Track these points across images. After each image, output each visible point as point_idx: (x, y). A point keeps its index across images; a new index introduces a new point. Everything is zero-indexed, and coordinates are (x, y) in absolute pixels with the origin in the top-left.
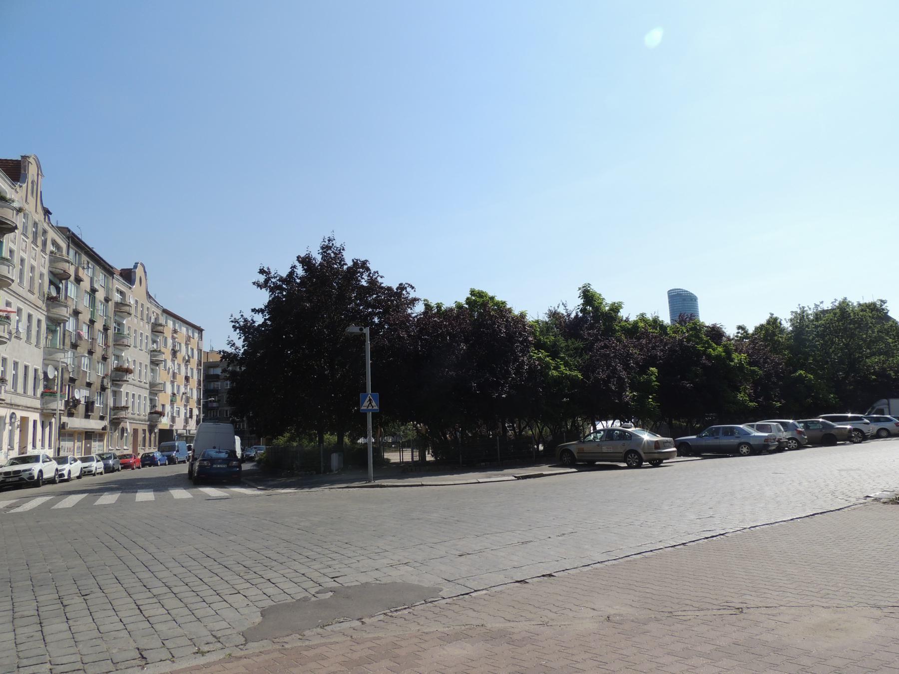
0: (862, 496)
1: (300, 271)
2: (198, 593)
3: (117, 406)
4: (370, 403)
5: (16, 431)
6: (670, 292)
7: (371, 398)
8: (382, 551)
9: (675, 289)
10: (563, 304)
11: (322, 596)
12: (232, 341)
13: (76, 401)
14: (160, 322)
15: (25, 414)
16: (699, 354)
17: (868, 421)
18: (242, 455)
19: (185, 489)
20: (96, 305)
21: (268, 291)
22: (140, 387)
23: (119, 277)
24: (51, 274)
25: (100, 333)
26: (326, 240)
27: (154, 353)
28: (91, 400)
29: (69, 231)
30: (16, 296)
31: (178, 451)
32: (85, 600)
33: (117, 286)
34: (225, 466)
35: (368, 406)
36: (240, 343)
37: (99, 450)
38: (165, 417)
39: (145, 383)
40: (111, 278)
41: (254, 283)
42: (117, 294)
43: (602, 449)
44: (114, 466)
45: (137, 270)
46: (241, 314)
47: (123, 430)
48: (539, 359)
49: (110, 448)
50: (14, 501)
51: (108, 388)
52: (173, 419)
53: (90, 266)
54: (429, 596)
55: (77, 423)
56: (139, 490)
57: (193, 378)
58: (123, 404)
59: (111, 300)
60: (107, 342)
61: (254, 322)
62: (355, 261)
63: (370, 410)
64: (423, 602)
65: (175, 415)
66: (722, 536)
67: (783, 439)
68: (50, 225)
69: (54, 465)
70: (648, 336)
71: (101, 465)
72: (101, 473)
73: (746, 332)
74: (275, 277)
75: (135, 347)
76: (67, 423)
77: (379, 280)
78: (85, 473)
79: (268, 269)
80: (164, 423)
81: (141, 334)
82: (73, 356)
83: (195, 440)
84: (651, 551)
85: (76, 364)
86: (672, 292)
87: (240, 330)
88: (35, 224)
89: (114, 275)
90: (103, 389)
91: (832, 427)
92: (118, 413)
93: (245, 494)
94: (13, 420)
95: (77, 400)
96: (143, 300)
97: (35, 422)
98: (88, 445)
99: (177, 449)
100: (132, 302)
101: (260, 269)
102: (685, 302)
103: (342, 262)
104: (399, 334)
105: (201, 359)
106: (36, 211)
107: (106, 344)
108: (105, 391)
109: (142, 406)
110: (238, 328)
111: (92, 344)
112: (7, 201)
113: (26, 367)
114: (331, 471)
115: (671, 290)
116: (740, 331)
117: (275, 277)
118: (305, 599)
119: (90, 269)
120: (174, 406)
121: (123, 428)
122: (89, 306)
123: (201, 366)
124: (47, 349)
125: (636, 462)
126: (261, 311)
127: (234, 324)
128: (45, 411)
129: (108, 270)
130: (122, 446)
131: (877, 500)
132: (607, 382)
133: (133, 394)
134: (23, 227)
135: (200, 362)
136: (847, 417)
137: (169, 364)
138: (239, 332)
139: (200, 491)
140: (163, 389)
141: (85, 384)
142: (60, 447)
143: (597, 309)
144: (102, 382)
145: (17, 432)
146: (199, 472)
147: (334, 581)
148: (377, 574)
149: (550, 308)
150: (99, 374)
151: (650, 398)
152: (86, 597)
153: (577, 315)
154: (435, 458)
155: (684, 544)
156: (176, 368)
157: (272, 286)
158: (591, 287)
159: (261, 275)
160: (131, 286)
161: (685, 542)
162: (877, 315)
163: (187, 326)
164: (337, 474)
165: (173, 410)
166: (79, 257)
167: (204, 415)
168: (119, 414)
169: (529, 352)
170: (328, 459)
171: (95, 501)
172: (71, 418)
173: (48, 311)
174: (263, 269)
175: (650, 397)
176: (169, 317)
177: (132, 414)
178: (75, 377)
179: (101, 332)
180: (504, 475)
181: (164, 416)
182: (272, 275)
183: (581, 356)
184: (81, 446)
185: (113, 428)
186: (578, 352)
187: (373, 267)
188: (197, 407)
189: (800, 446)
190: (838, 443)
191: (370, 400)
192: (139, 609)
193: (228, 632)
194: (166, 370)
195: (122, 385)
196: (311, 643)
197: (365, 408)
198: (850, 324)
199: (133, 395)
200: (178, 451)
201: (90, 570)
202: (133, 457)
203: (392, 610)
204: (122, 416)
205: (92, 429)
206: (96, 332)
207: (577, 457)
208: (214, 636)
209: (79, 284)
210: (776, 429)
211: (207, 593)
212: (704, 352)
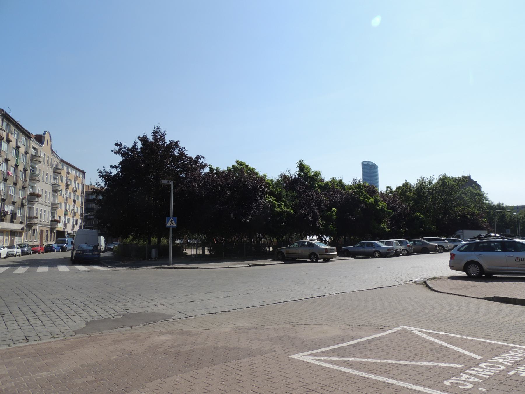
0: (408, 280)
1: (139, 145)
2: (58, 315)
3: (31, 216)
4: (172, 223)
6: (363, 163)
7: (172, 220)
8: (155, 299)
9: (365, 161)
10: (288, 170)
11: (116, 317)
12: (99, 183)
13: (5, 213)
14: (59, 167)
16: (360, 201)
17: (447, 242)
18: (105, 247)
19: (67, 266)
20: (19, 156)
21: (120, 155)
22: (45, 205)
23: (34, 140)
25: (21, 172)
26: (156, 128)
27: (55, 185)
28: (15, 212)
29: (3, 111)
31: (67, 244)
32: (2, 317)
33: (33, 145)
34: (90, 254)
35: (171, 224)
36: (103, 184)
37: (19, 242)
38: (60, 223)
39: (48, 203)
40: (29, 140)
41: (112, 151)
42: (32, 150)
43: (298, 252)
44: (28, 252)
45: (45, 136)
46: (104, 168)
47: (34, 230)
48: (270, 201)
49: (26, 240)
51: (25, 205)
52: (65, 225)
53: (16, 132)
54: (166, 318)
56: (40, 266)
57: (78, 201)
58: (35, 215)
59: (29, 153)
60: (25, 178)
61: (111, 173)
62: (171, 141)
63: (171, 226)
64: (163, 320)
65: (66, 222)
66: (323, 297)
67: (399, 249)
70: (334, 190)
71: (19, 250)
72: (19, 255)
73: (391, 190)
74: (125, 148)
75: (43, 181)
77: (186, 153)
78: (9, 255)
79: (121, 143)
80: (60, 227)
81: (47, 174)
82: (5, 185)
83: (75, 239)
84: (283, 302)
85: (6, 190)
86: (364, 162)
87: (103, 178)
89: (31, 138)
90: (23, 205)
91: (427, 244)
92: (31, 220)
93: (99, 270)
96: (49, 153)
98: (12, 239)
99: (66, 243)
100: (42, 155)
101: (116, 143)
102: (371, 169)
103: (164, 140)
104: (192, 184)
105: (84, 190)
107: (24, 179)
109: (46, 217)
110: (102, 176)
111: (16, 179)
114: (151, 258)
115: (363, 162)
116: (388, 189)
117: (125, 148)
118: (109, 318)
119: (16, 135)
120: (66, 217)
121: (34, 229)
122: (15, 156)
123: (83, 194)
125: (315, 259)
126: (116, 167)
127: (99, 174)
129: (28, 135)
130: (33, 240)
131: (415, 282)
132: (306, 215)
135: (83, 191)
136: (442, 239)
137: (64, 192)
138: (102, 179)
139: (75, 267)
140: (59, 207)
141: (11, 202)
143: (306, 174)
144: (22, 202)
146: (75, 257)
147: (126, 311)
148: (147, 309)
149: (282, 173)
151: (331, 225)
152: (3, 316)
153: (295, 177)
154: (210, 253)
155: (301, 300)
156: (68, 195)
157: (123, 153)
158: (304, 162)
159: (116, 146)
160: (41, 145)
161: (302, 299)
162: (462, 184)
163: (76, 170)
164: (154, 260)
165: (66, 220)
166: (9, 127)
167: (84, 223)
168: (32, 221)
169: (264, 197)
170: (150, 253)
171: (13, 271)
174: (117, 143)
175: (332, 224)
177: (40, 221)
178: (5, 198)
179: (22, 172)
180: (243, 264)
181: (60, 223)
182: (123, 147)
183: (295, 200)
184: (8, 239)
185: (28, 229)
186: (293, 198)
187: (181, 145)
188: (80, 218)
189: (409, 254)
190: (430, 252)
191: (172, 221)
192: (28, 321)
193: (69, 330)
194: (62, 196)
195: (34, 204)
196: (103, 334)
197: (169, 225)
198: (446, 188)
199: (41, 210)
200: (67, 244)
201: (6, 304)
202: (40, 247)
203: (147, 323)
204: (34, 222)
205: (15, 229)
206: (19, 172)
207: (285, 256)
208: (62, 332)
209: (9, 143)
210: (395, 244)
211: (62, 314)
212: (364, 201)
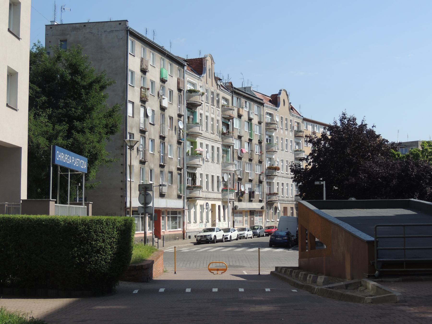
5: (209, 212)
15: (213, 202)
22: (287, 178)
24: (223, 118)
28: (252, 191)
30: (205, 138)
34: (281, 239)
45: (281, 96)
49: (267, 220)
50: (199, 248)
55: (245, 205)
58: (275, 191)
68: (221, 90)
69: (222, 233)
72: (251, 238)
76: (238, 206)
81: (287, 140)
88: (212, 93)
90: (261, 182)
94: (207, 207)
95: (243, 192)
97: (219, 206)
106: (212, 86)
108: (262, 183)
109: (290, 191)
112: (196, 92)
113: (213, 176)
124: (223, 163)
128: (224, 200)
133: (282, 183)
134: (206, 97)
142: (235, 220)
144: (260, 178)
145: (210, 213)
150: (258, 173)
172: (240, 203)
173: (223, 141)
176: (308, 123)
179: (257, 145)
199: (283, 184)
204: (273, 200)
